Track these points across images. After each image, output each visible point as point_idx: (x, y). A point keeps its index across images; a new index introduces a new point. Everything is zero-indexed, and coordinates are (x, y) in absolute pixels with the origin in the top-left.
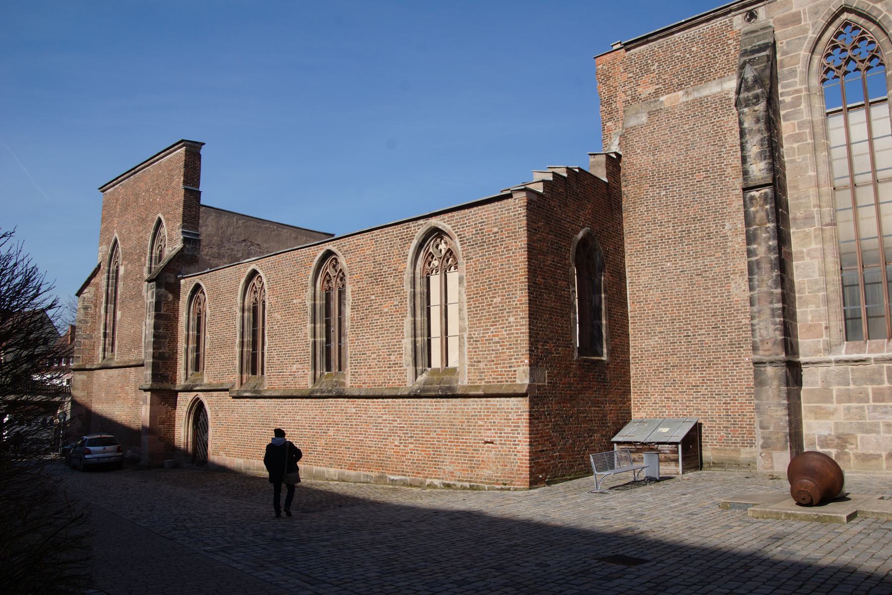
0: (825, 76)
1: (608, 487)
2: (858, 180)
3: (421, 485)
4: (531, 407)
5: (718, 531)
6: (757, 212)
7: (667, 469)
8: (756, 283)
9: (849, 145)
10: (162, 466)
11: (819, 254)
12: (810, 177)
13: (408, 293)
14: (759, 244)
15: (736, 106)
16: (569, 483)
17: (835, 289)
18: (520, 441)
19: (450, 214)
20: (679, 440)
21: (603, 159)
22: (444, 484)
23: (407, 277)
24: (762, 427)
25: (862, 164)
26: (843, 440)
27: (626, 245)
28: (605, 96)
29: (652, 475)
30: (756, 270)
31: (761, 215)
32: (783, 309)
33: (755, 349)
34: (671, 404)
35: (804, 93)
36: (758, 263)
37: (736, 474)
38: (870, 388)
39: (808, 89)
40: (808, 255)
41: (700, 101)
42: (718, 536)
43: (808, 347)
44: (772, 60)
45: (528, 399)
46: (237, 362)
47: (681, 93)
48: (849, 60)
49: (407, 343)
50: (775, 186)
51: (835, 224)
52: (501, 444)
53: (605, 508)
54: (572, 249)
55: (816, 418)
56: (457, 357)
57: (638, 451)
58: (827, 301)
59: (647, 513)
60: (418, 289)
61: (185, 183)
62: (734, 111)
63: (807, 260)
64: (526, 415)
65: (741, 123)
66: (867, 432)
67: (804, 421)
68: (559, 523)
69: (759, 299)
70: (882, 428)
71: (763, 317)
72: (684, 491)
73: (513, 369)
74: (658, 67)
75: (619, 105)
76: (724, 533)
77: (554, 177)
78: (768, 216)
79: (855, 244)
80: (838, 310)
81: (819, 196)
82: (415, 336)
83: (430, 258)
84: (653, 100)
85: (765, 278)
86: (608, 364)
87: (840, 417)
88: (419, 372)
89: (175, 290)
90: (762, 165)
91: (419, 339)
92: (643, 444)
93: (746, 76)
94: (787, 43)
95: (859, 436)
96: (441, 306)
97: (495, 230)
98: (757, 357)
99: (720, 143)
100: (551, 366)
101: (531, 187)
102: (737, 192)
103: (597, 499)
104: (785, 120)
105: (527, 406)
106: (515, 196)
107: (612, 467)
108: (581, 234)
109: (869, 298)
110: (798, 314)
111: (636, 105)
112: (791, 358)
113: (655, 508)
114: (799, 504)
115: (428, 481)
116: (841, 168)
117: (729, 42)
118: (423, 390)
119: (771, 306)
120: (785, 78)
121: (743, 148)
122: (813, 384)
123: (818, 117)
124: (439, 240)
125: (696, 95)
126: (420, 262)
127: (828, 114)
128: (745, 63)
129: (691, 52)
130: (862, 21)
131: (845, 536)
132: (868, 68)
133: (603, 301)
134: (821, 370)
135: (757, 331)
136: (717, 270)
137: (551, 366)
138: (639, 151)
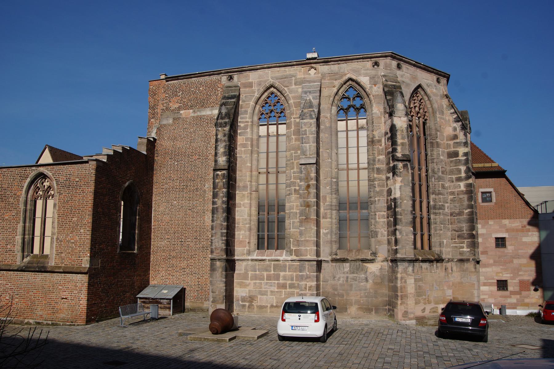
0: (261, 117)
3: (21, 323)
4: (90, 280)
8: (215, 219)
11: (248, 206)
13: (22, 209)
16: (109, 321)
17: (254, 224)
19: (52, 167)
20: (171, 297)
22: (36, 322)
23: (22, 199)
24: (213, 292)
25: (272, 163)
28: (152, 104)
29: (153, 316)
31: (221, 184)
32: (227, 233)
33: (212, 252)
35: (250, 123)
36: (217, 208)
38: (265, 274)
39: (252, 122)
40: (243, 205)
41: (201, 117)
43: (239, 251)
44: (237, 105)
47: (191, 111)
54: (121, 193)
56: (48, 248)
58: (250, 229)
60: (29, 207)
63: (243, 208)
65: (217, 135)
66: (262, 295)
70: (269, 293)
75: (159, 111)
77: (114, 152)
78: (224, 185)
80: (255, 234)
81: (251, 176)
82: (24, 234)
83: (37, 190)
86: (137, 255)
87: (251, 287)
88: (25, 256)
90: (224, 158)
91: (27, 236)
92: (153, 299)
94: (245, 96)
95: (259, 296)
96: (42, 218)
97: (77, 180)
99: (207, 142)
103: (120, 331)
104: (240, 136)
105: (87, 279)
106: (90, 162)
108: (127, 184)
109: (270, 229)
112: (229, 258)
114: (213, 334)
115: (26, 321)
117: (219, 89)
118: (27, 267)
124: (44, 180)
125: (199, 114)
126: (31, 192)
129: (199, 90)
130: (279, 94)
134: (245, 263)
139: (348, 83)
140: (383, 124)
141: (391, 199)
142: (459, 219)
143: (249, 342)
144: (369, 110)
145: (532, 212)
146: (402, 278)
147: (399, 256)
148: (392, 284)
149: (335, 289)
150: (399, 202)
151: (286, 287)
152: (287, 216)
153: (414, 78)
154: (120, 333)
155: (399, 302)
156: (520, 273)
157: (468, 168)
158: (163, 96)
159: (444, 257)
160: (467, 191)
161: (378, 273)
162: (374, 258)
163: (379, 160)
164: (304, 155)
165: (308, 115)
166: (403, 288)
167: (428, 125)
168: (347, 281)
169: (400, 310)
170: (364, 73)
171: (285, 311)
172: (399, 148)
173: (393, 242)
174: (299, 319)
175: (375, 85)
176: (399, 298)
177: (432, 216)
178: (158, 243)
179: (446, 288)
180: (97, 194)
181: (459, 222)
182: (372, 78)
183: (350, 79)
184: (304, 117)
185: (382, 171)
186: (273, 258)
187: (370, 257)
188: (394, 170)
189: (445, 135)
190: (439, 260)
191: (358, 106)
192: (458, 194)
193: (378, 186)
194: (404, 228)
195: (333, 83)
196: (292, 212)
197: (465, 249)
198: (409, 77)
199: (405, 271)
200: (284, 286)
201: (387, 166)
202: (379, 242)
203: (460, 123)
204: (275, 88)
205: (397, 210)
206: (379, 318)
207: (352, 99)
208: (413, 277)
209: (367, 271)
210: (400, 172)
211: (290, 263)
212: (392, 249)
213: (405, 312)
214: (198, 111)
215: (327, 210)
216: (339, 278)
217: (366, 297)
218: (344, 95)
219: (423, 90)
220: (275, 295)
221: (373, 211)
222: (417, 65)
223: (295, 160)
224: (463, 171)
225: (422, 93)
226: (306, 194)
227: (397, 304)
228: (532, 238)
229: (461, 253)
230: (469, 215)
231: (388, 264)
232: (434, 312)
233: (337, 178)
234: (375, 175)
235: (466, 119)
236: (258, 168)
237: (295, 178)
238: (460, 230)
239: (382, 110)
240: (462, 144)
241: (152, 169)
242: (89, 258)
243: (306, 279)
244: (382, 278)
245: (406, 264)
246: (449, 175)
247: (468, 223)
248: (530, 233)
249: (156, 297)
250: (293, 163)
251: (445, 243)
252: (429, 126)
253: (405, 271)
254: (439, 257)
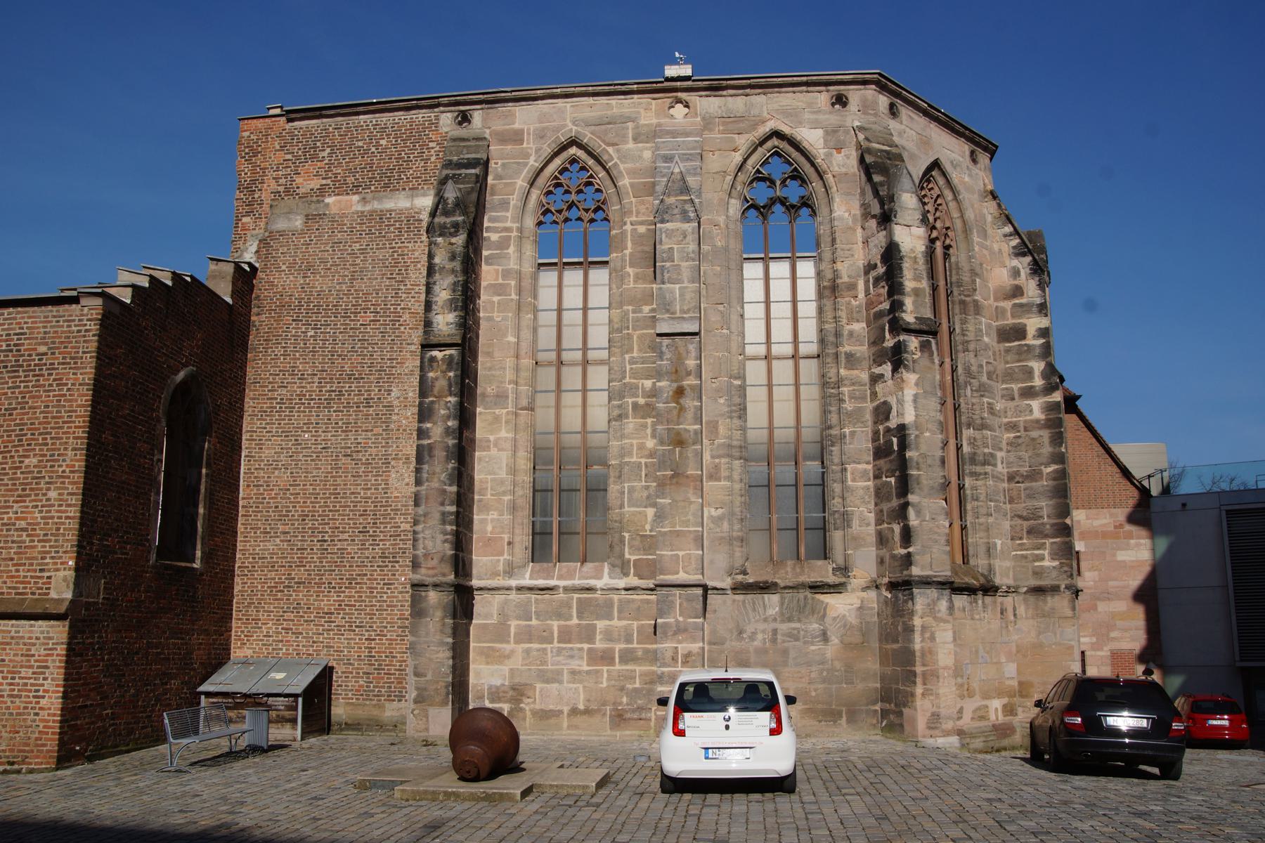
0: (542, 218)
1: (188, 762)
2: (566, 356)
5: (354, 821)
6: (437, 379)
7: (279, 733)
8: (425, 475)
9: (560, 310)
11: (508, 445)
12: (509, 343)
14: (435, 423)
15: (428, 232)
16: (125, 758)
18: (45, 691)
20: (299, 690)
21: (230, 269)
24: (417, 674)
26: (518, 692)
27: (246, 400)
28: (246, 177)
29: (258, 743)
30: (427, 458)
31: (441, 384)
32: (458, 513)
33: (415, 565)
34: (291, 637)
35: (515, 234)
36: (430, 448)
37: (377, 740)
38: (555, 625)
39: (520, 230)
40: (496, 445)
41: (381, 215)
42: (354, 828)
44: (482, 181)
45: (67, 623)
47: (356, 198)
48: (571, 205)
50: (464, 348)
51: (532, 410)
52: (11, 696)
53: (184, 794)
55: (488, 663)
57: (237, 706)
58: (513, 508)
59: (249, 800)
62: (424, 238)
63: (494, 451)
64: (61, 650)
65: (431, 256)
66: (547, 682)
67: (471, 666)
68: (108, 823)
69: (427, 498)
70: (566, 677)
71: (431, 523)
72: (304, 766)
73: (46, 574)
74: (330, 155)
75: (266, 196)
76: (363, 824)
77: (150, 282)
78: (450, 386)
79: (553, 437)
80: (526, 521)
81: (517, 369)
84: (315, 199)
85: (438, 470)
86: (202, 574)
87: (517, 662)
90: (451, 317)
92: (245, 696)
93: (446, 195)
94: (503, 165)
95: (539, 686)
97: (43, 349)
98: (417, 577)
99: (399, 278)
100: (111, 573)
101: (112, 291)
102: (413, 348)
103: (171, 781)
104: (487, 264)
105: (65, 635)
106: (84, 301)
107: (196, 732)
110: (475, 522)
111: (289, 201)
112: (462, 581)
113: (262, 792)
114: (462, 779)
116: (547, 338)
117: (431, 145)
119: (442, 508)
120: (494, 209)
121: (429, 291)
122: (487, 616)
123: (528, 268)
125: (376, 205)
127: (541, 265)
128: (447, 178)
129: (378, 145)
130: (591, 162)
131: (519, 819)
132: (592, 221)
133: (203, 480)
134: (498, 598)
135: (421, 542)
136: (374, 451)
137: (111, 573)
138: (284, 267)
139: (769, 144)
140: (860, 244)
141: (888, 430)
142: (1031, 488)
143: (576, 800)
144: (823, 211)
145: (1136, 493)
146: (924, 628)
147: (916, 571)
148: (895, 646)
150: (912, 434)
151: (613, 659)
152: (613, 474)
153: (925, 142)
154: (173, 785)
155: (919, 690)
156: (1113, 635)
158: (276, 158)
159: (997, 581)
160: (1048, 420)
161: (853, 619)
162: (843, 580)
163: (851, 334)
164: (668, 311)
165: (676, 211)
166: (929, 653)
167: (953, 259)
168: (774, 640)
169: (921, 710)
170: (809, 119)
171: (683, 706)
172: (909, 302)
173: (897, 537)
174: (727, 727)
175: (839, 150)
176: (919, 680)
177: (968, 482)
178: (255, 545)
179: (1003, 660)
180: (101, 391)
181: (1030, 497)
182: (831, 132)
183: (777, 134)
184: (666, 217)
185: (859, 360)
186: (577, 582)
187: (831, 579)
188: (897, 358)
190: (989, 589)
191: (794, 200)
192: (1026, 429)
193: (851, 398)
194: (925, 502)
195: (733, 140)
196: (628, 463)
197: (1047, 563)
198: (919, 140)
199: (931, 609)
200: (606, 658)
201: (874, 349)
202: (855, 539)
203: (1028, 259)
204: (581, 146)
205: (908, 454)
206: (858, 736)
207: (778, 183)
208: (949, 626)
209: (824, 616)
210: (914, 361)
211: (624, 595)
212: (893, 557)
213: (933, 714)
214: (374, 198)
215: (719, 457)
216: (754, 633)
217: (824, 681)
218: (758, 171)
219: (944, 174)
220: (581, 682)
221: (836, 460)
222: (930, 113)
223: (634, 329)
224: (1037, 373)
225: (941, 181)
226: (675, 412)
227: (913, 695)
228: (1138, 553)
229: (1038, 573)
230: (1054, 479)
231: (879, 595)
232: (982, 718)
233: (744, 378)
234: (843, 372)
235: (1043, 250)
236: (534, 351)
237: (635, 375)
238: (1034, 515)
239: (857, 211)
240: (1035, 309)
241: (243, 346)
242: (72, 573)
243: (675, 634)
244: (864, 632)
245: (933, 593)
246: (1003, 382)
247: (1052, 498)
248: (1132, 541)
249: (254, 691)
250: (629, 337)
251: (999, 547)
252: (957, 263)
253: (931, 609)
254: (988, 581)
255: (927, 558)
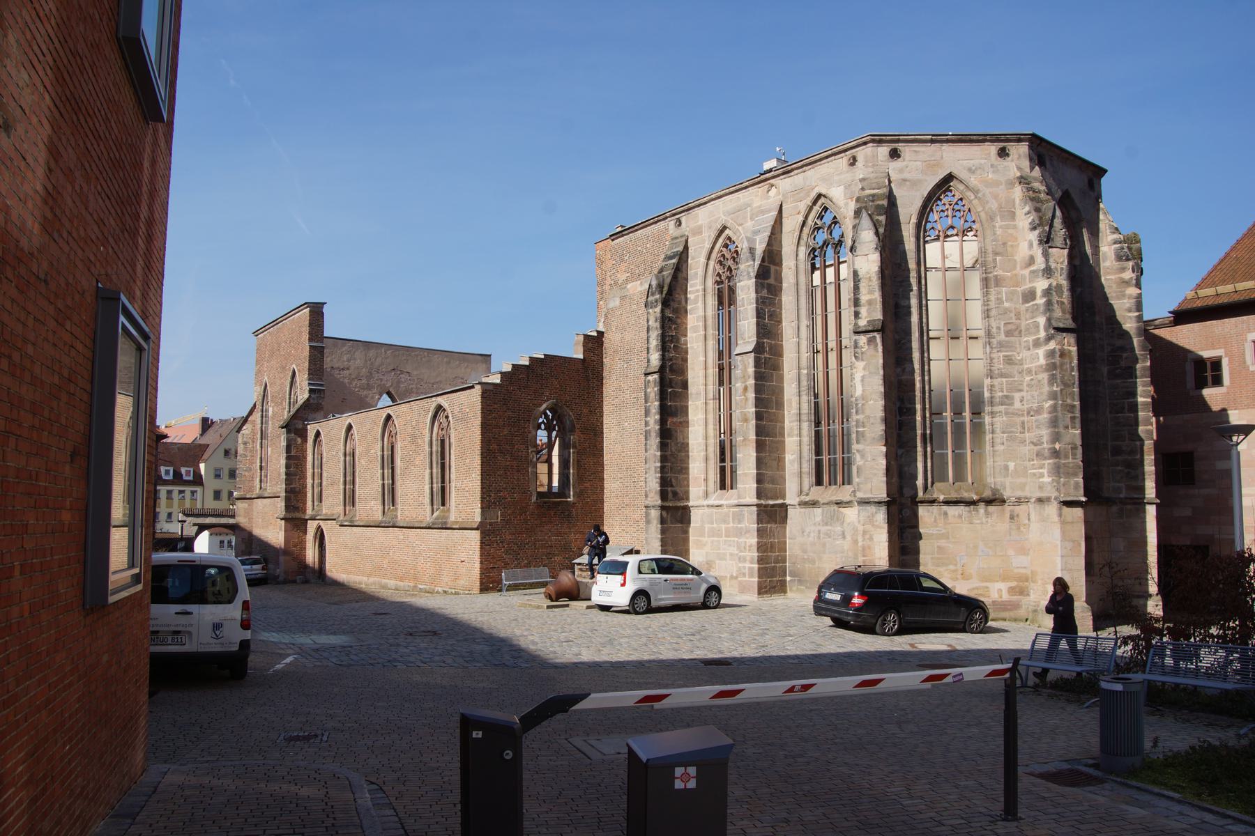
10: (294, 582)
46: (342, 497)
49: (427, 487)
61: (310, 340)
89: (303, 434)
96: (929, 360)
114: (840, 623)
139: (820, 203)
146: (865, 532)
149: (805, 551)
157: (1049, 320)
159: (1006, 494)
168: (819, 537)
179: (1011, 552)
180: (485, 426)
181: (1037, 427)
189: (1018, 258)
190: (995, 500)
194: (868, 448)
225: (961, 187)
255: (869, 486)
